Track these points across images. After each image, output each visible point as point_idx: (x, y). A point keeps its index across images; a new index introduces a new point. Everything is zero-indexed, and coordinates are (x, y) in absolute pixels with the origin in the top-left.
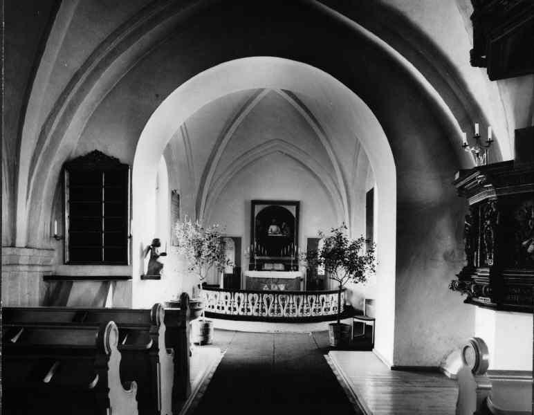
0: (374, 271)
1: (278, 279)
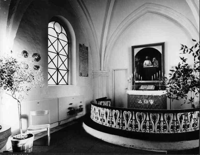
1: (149, 96)
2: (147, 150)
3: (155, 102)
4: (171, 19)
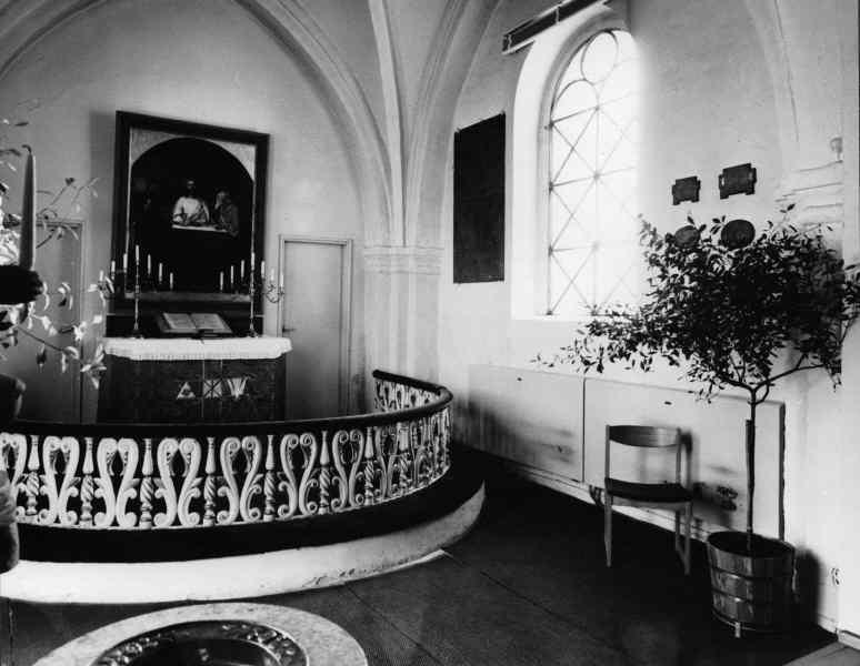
0: (710, 402)
2: (395, 568)
3: (249, 388)
4: (281, 38)
